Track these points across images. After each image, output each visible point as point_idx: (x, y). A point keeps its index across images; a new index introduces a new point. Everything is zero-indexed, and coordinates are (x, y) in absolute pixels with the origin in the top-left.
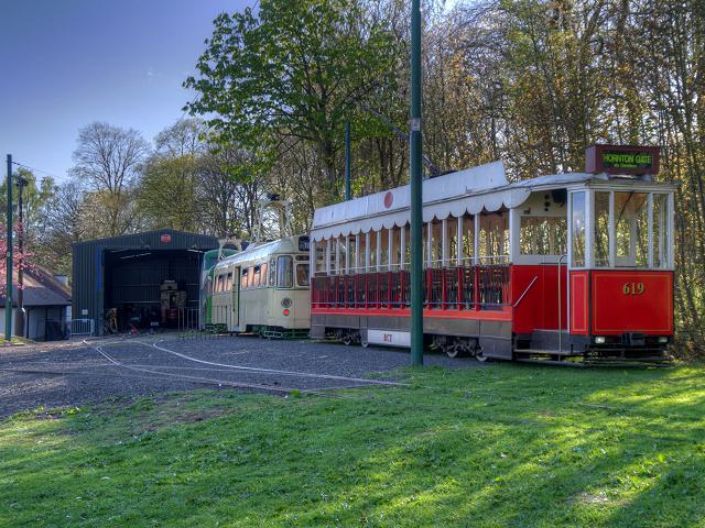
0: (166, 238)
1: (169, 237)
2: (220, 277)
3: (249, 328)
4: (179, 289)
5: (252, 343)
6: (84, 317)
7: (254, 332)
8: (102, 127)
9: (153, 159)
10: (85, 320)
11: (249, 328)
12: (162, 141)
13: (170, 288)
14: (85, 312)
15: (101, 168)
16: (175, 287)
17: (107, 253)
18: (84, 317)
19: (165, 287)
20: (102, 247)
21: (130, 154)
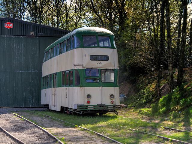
5: (63, 116)
7: (64, 110)
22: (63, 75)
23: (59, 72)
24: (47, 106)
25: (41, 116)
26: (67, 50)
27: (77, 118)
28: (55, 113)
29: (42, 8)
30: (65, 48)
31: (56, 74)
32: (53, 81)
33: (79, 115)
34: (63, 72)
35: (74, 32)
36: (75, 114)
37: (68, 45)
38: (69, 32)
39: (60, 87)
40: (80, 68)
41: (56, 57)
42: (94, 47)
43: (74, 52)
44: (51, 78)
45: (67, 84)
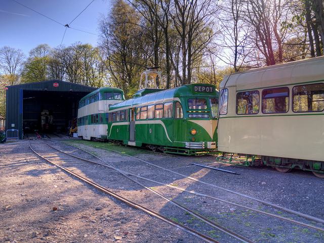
0: (56, 85)
1: (58, 84)
2: (240, 95)
3: (92, 138)
4: (50, 115)
5: (92, 143)
6: (13, 128)
7: (93, 139)
8: (7, 48)
9: (29, 59)
10: (13, 130)
11: (92, 138)
12: (31, 53)
13: (45, 113)
14: (13, 125)
15: (7, 65)
16: (48, 113)
17: (24, 91)
18: (13, 128)
19: (43, 113)
20: (22, 89)
21: (18, 60)
22: (92, 117)
23: (89, 116)
24: (82, 137)
25: (79, 143)
26: (94, 101)
27: (101, 143)
28: (143, 155)
29: (76, 71)
30: (89, 102)
31: (87, 116)
32: (129, 116)
33: (102, 142)
34: (92, 115)
35: (98, 90)
36: (100, 141)
37: (95, 98)
38: (89, 93)
39: (90, 124)
40: (103, 112)
41: (87, 106)
42: (112, 99)
43: (98, 105)
44: (125, 113)
45: (95, 122)
